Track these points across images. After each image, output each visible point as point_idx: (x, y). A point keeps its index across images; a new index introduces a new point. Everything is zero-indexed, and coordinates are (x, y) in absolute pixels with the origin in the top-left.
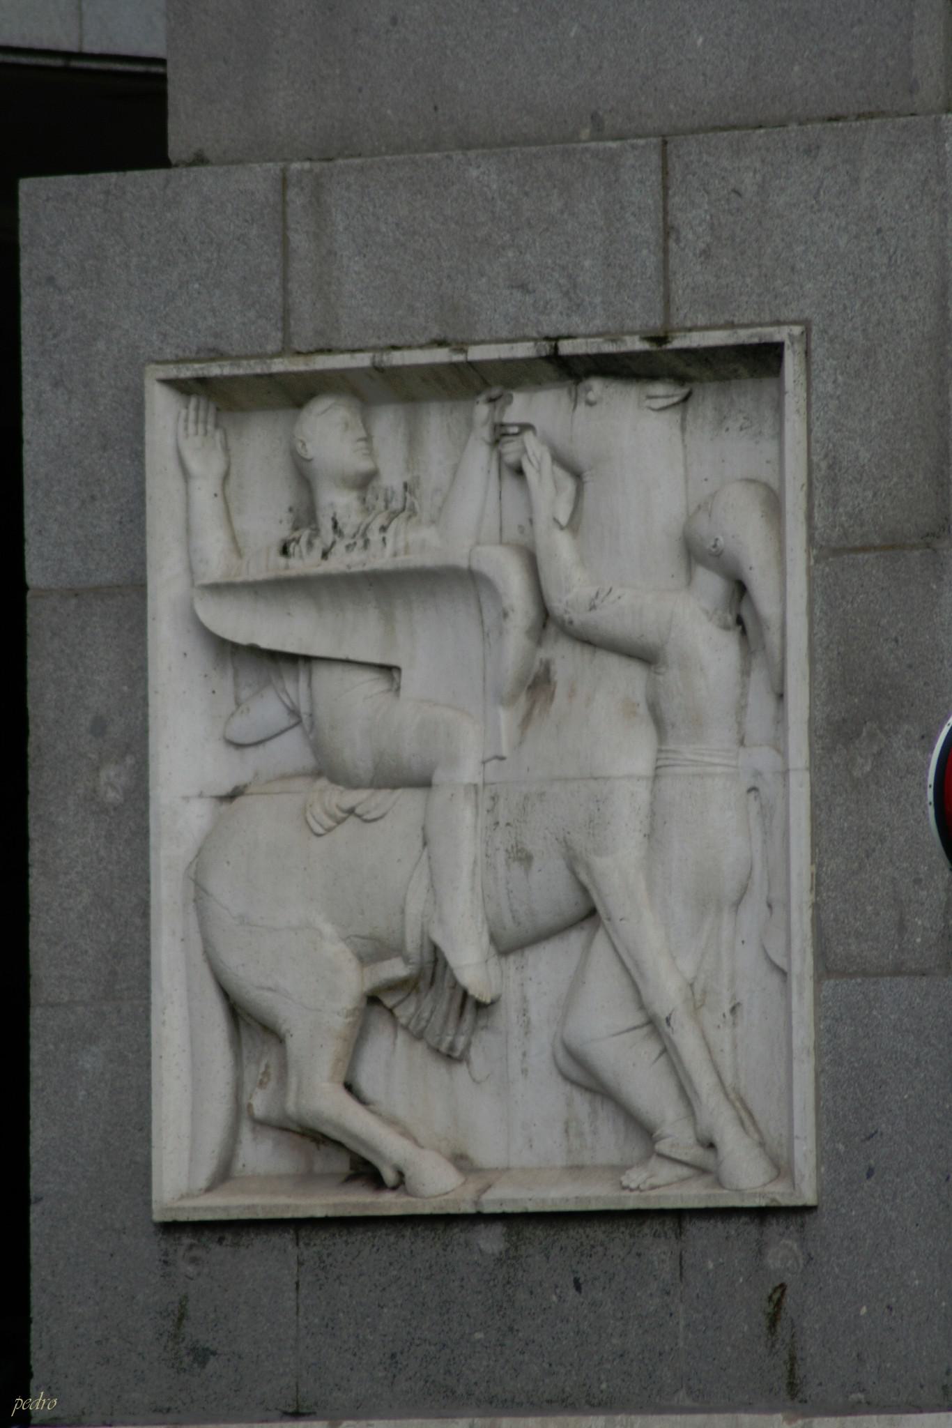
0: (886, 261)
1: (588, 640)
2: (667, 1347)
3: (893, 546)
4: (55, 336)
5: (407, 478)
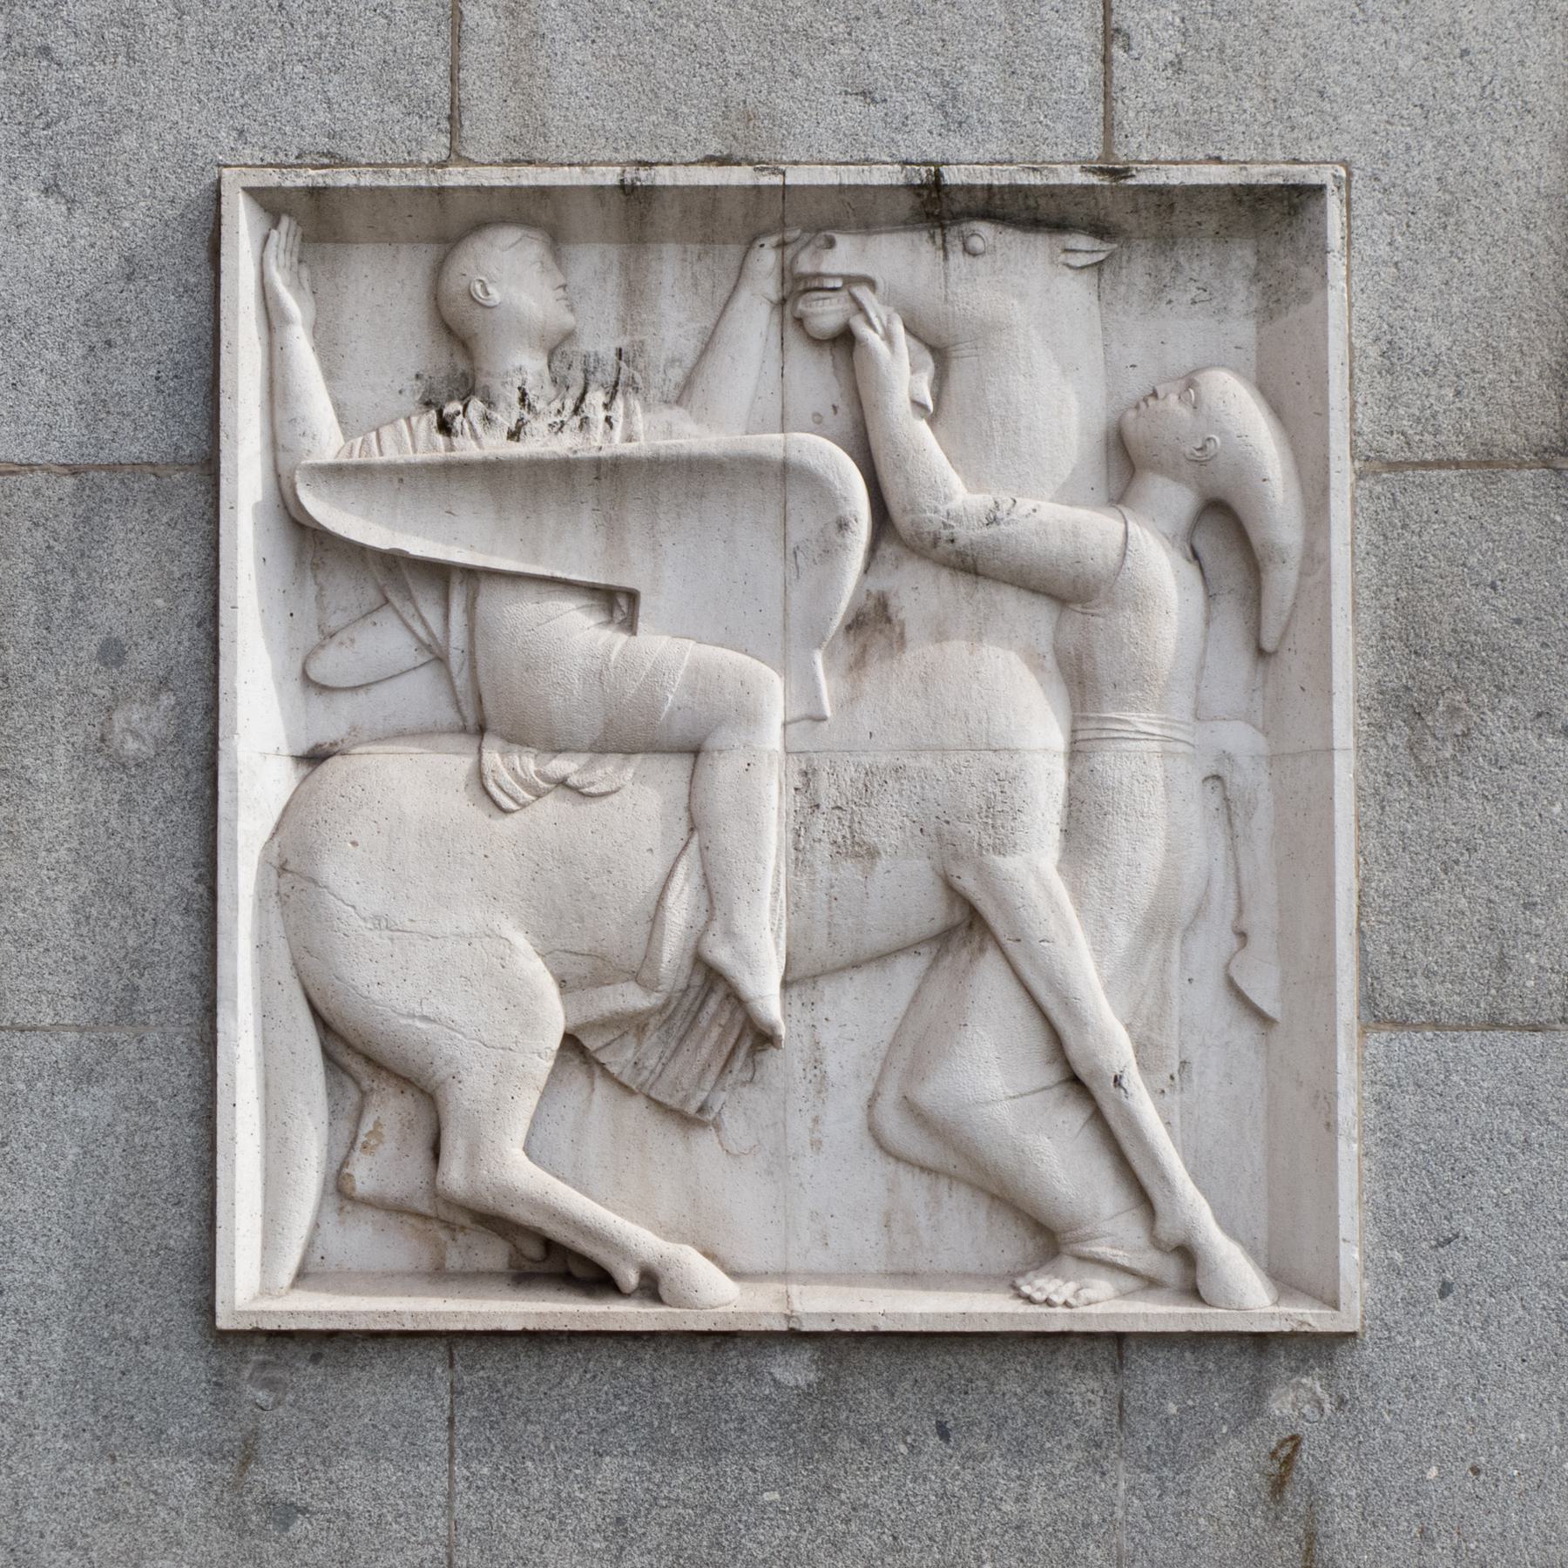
0: (1476, 90)
1: (969, 565)
2: (1096, 1517)
3: (1487, 462)
4: (48, 126)
5: (623, 342)
